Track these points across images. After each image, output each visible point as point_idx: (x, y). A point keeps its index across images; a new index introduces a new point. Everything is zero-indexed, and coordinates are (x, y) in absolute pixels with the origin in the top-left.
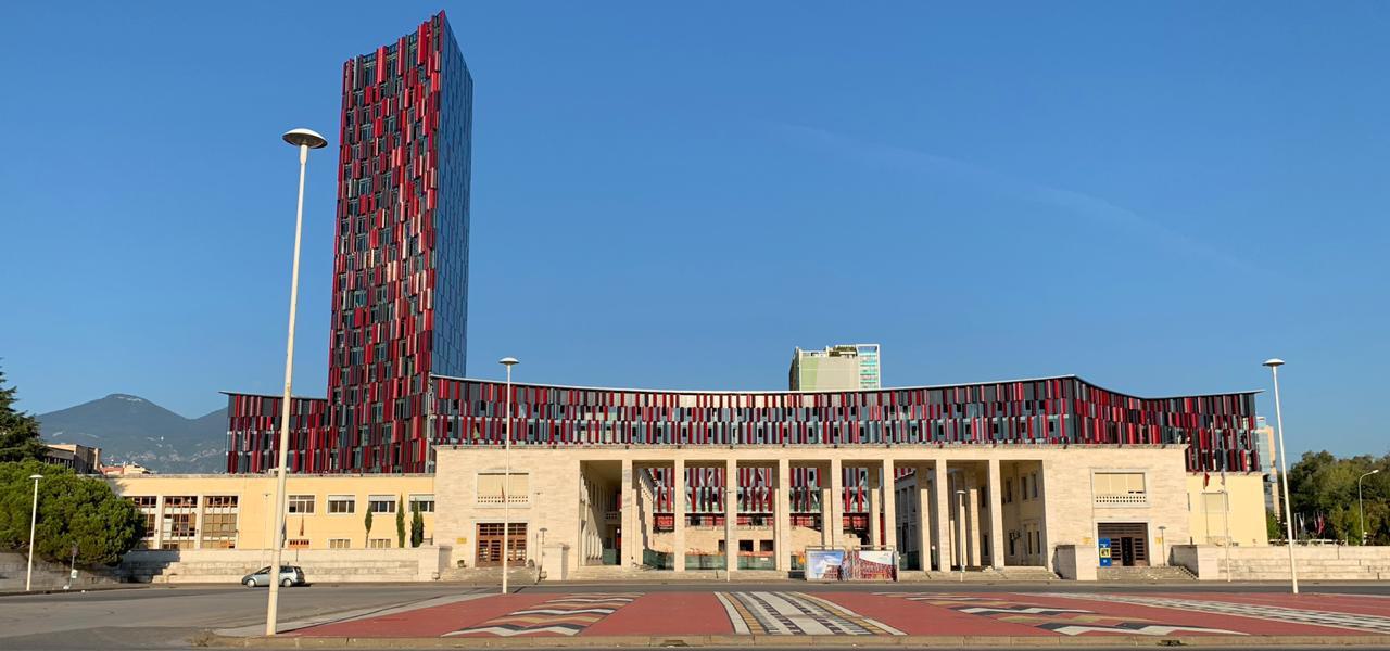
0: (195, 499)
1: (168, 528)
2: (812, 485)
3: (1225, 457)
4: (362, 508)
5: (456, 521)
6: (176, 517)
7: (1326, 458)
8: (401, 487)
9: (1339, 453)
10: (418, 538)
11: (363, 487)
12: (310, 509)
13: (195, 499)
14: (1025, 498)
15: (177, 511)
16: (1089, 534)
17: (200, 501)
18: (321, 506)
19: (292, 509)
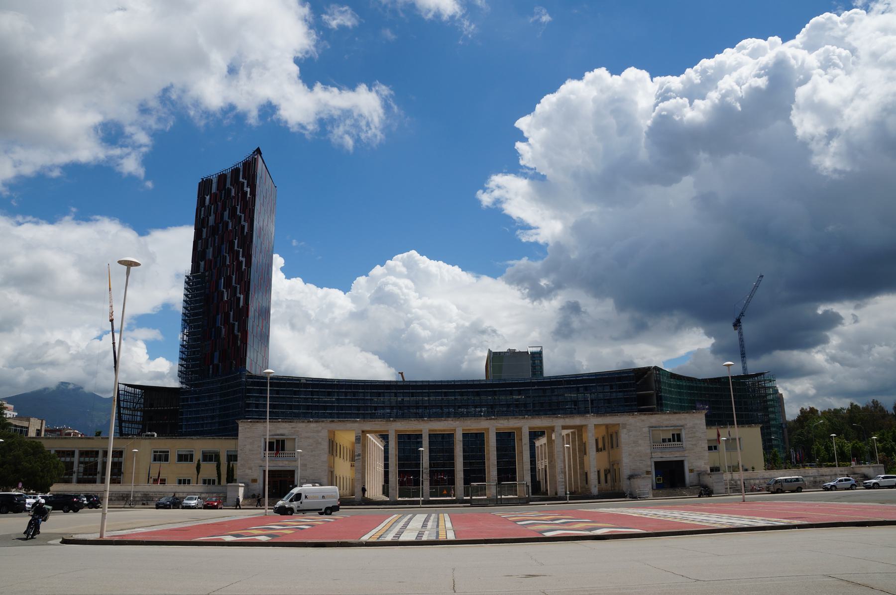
0: (97, 452)
1: (81, 470)
2: (329, 128)
3: (492, 472)
4: (198, 456)
5: (250, 468)
6: (86, 463)
7: (813, 411)
8: (220, 445)
9: (820, 409)
10: (231, 478)
11: (199, 446)
12: (166, 460)
13: (97, 452)
14: (612, 447)
15: (87, 459)
16: (649, 469)
17: (77, 454)
18: (173, 457)
19: (155, 460)
